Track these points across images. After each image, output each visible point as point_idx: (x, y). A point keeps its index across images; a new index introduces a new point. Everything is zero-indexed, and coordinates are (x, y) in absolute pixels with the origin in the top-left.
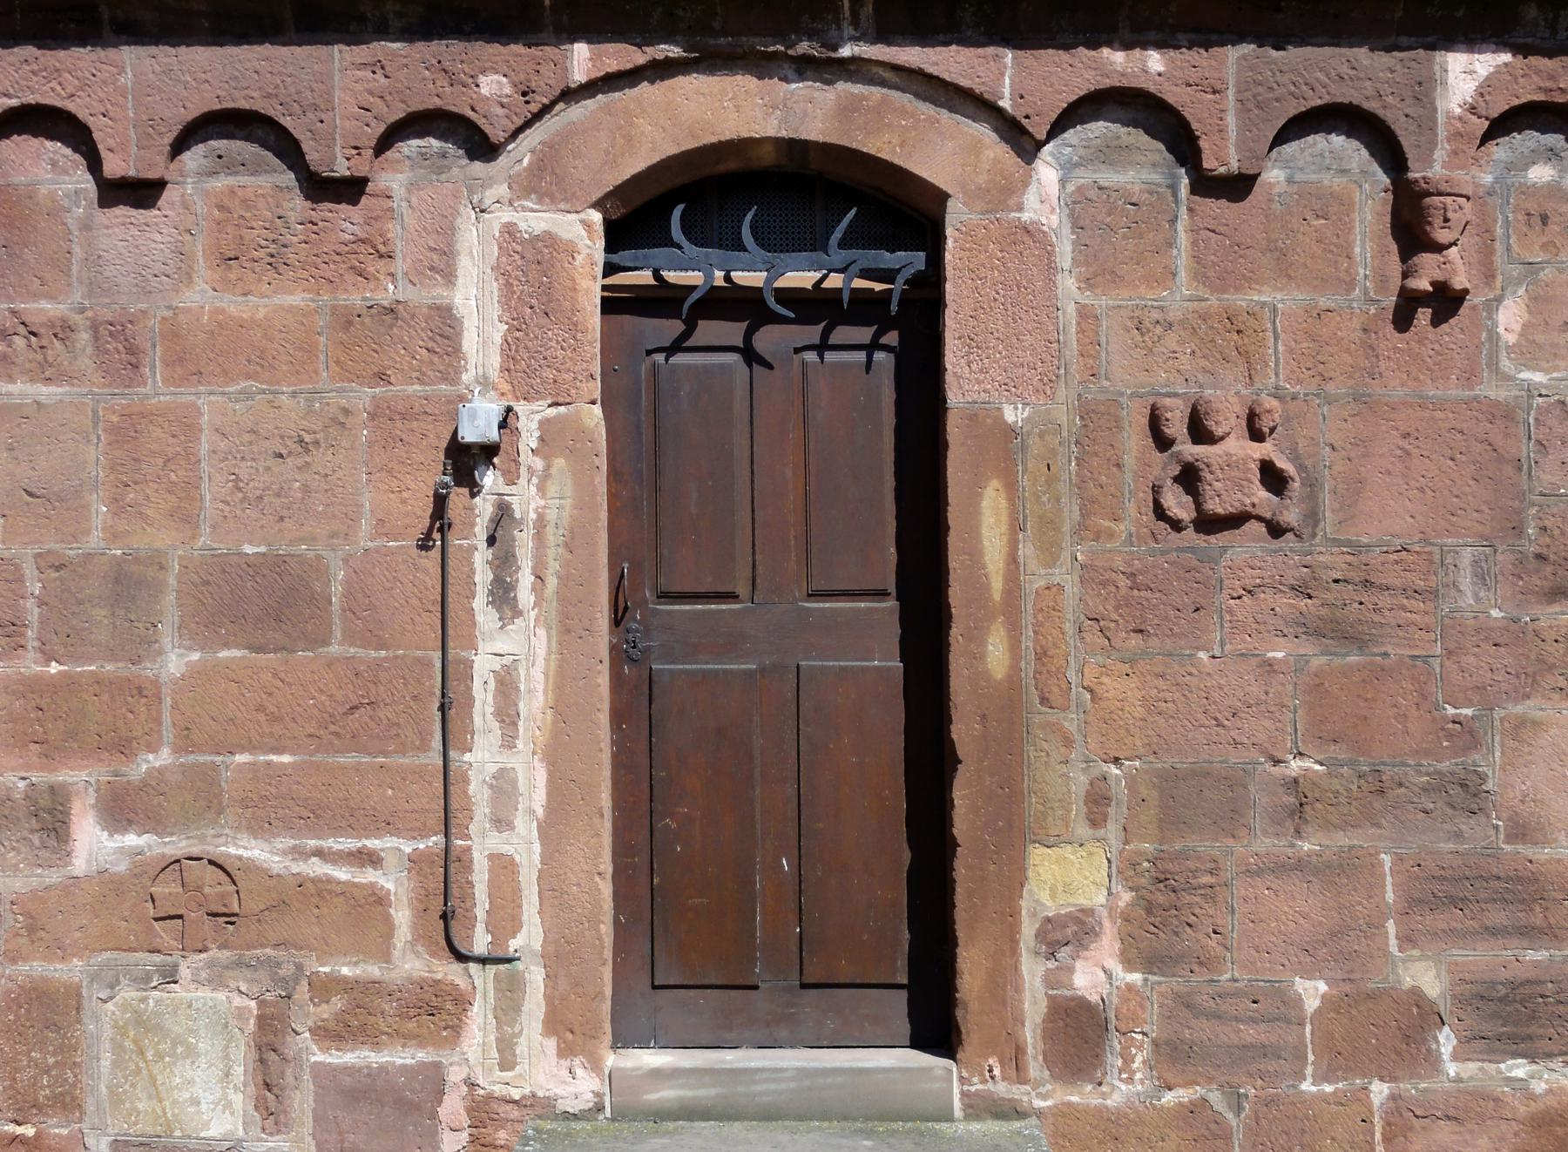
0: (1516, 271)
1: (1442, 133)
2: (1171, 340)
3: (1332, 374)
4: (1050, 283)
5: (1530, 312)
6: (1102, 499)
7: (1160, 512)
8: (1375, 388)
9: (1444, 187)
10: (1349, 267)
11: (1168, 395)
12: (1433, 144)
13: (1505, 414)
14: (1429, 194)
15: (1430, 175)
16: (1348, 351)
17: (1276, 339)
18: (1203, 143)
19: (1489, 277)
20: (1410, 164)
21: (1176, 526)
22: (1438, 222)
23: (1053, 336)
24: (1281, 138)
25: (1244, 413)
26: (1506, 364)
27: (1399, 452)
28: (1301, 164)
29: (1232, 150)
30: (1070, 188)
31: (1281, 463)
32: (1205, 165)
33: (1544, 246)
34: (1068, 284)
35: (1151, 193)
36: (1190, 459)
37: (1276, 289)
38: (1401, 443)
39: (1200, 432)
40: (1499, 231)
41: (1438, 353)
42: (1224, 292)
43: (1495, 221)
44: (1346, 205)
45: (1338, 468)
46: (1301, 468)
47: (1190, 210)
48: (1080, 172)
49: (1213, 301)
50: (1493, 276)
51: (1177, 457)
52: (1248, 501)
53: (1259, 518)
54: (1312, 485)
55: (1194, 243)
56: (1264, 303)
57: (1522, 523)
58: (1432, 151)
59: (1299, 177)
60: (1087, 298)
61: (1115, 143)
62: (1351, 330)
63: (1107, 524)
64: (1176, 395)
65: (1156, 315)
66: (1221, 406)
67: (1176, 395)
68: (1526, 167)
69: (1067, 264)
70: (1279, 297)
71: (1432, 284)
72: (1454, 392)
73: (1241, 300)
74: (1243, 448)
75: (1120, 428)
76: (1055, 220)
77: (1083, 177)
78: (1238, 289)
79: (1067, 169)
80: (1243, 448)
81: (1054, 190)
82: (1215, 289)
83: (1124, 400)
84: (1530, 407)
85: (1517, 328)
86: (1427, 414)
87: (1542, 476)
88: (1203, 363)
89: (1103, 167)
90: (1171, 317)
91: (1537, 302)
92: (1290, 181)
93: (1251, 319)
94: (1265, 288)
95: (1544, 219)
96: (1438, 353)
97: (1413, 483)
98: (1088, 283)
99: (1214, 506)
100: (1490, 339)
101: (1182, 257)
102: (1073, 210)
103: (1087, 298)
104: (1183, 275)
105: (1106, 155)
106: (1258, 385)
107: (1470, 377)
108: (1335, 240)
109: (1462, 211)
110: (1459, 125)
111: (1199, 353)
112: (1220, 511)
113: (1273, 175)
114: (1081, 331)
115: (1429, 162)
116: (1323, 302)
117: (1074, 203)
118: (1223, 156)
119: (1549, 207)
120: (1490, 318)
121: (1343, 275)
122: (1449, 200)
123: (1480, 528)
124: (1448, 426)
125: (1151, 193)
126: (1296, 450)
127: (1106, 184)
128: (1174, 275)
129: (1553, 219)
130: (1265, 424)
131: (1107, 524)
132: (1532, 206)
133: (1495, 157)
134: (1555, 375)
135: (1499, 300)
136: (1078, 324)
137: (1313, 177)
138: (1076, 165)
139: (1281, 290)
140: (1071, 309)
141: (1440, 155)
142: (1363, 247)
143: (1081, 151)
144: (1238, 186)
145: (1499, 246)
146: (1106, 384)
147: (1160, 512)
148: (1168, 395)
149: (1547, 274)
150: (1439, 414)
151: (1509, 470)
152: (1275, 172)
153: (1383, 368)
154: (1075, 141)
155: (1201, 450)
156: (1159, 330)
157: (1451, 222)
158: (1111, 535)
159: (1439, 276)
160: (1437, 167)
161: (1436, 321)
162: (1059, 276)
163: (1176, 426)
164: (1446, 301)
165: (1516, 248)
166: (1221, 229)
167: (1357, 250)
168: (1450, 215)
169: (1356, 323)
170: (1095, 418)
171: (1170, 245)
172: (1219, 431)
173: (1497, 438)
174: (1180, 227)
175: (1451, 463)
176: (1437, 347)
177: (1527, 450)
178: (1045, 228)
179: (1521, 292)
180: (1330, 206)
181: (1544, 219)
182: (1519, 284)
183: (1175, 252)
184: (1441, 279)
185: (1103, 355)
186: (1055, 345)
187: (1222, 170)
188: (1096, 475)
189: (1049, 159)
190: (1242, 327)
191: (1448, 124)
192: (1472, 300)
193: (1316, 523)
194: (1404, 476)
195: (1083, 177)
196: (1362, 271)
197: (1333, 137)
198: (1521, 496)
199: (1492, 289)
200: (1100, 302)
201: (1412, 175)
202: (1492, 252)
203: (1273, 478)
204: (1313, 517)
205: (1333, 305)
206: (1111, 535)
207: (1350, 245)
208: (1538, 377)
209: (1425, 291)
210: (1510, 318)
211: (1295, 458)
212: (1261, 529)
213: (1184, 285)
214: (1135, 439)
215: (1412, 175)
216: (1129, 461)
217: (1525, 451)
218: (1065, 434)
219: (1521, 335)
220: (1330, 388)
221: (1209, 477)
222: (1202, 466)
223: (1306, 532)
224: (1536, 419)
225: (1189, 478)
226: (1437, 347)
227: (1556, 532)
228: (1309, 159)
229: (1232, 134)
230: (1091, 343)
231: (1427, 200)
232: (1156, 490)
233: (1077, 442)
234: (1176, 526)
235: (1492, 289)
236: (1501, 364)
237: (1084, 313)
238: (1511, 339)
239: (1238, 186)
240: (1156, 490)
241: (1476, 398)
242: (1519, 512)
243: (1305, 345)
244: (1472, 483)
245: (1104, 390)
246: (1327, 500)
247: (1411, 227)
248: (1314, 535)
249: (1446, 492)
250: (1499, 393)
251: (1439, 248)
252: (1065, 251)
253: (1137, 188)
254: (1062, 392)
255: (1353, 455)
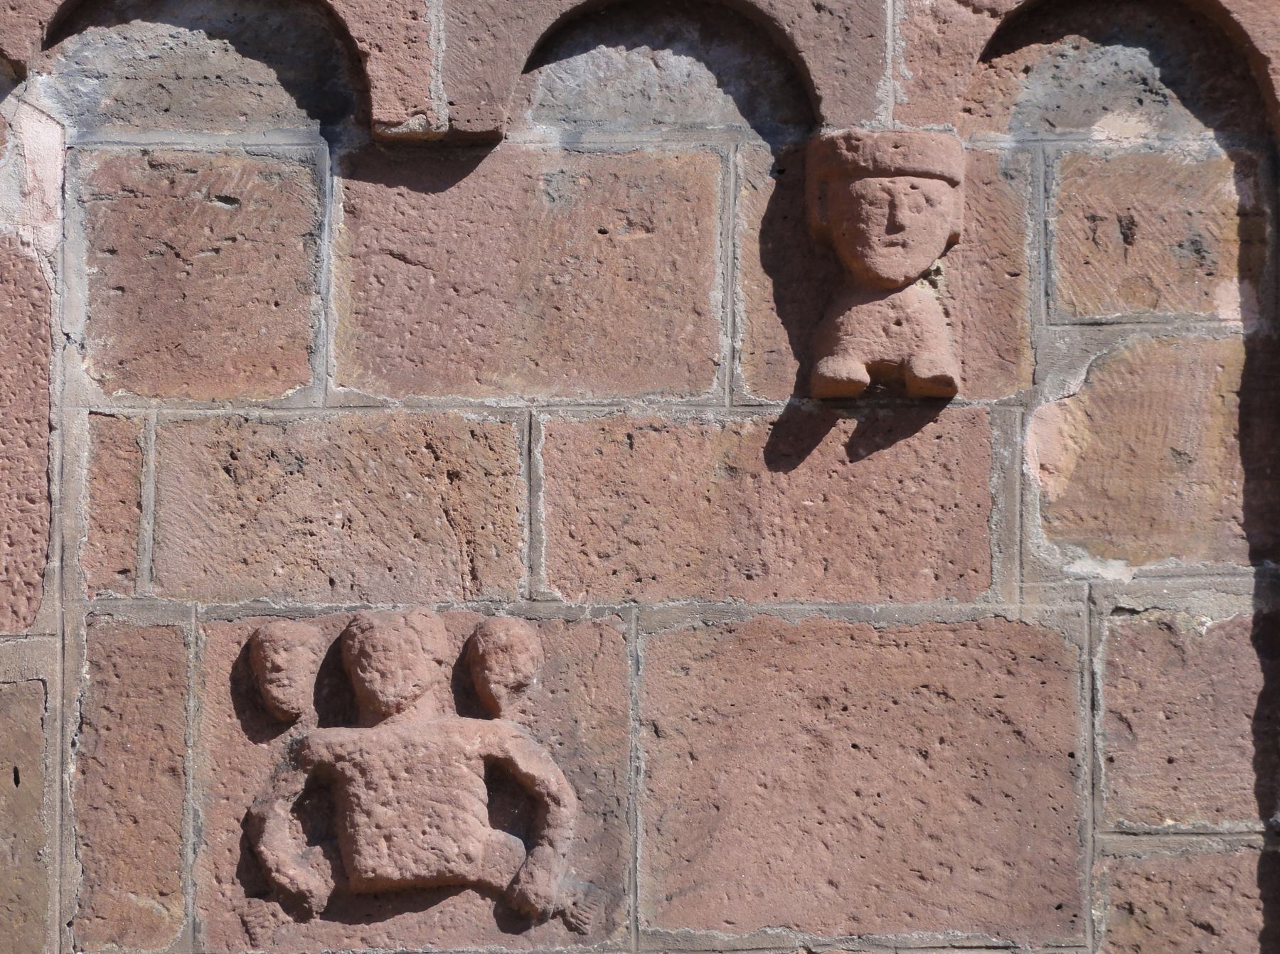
0: (1064, 339)
1: (894, 42)
2: (301, 496)
3: (656, 567)
4: (36, 371)
5: (1095, 430)
6: (133, 846)
7: (256, 877)
8: (755, 602)
9: (889, 157)
10: (698, 331)
11: (290, 615)
12: (874, 67)
13: (1039, 654)
14: (864, 173)
15: (858, 131)
16: (693, 516)
17: (533, 489)
18: (374, 68)
19: (1007, 354)
20: (825, 109)
21: (297, 905)
22: (876, 232)
23: (37, 487)
24: (549, 49)
25: (450, 652)
26: (1039, 540)
27: (804, 739)
28: (596, 111)
29: (437, 83)
30: (89, 165)
31: (536, 763)
32: (378, 114)
33: (1127, 288)
34: (76, 375)
35: (267, 175)
36: (327, 756)
37: (533, 379)
38: (807, 716)
39: (346, 691)
40: (1030, 255)
41: (893, 520)
42: (422, 388)
43: (1020, 233)
44: (693, 199)
45: (664, 778)
46: (581, 775)
47: (351, 211)
48: (114, 132)
49: (397, 407)
50: (1017, 351)
51: (298, 755)
52: (452, 849)
53: (483, 888)
54: (607, 815)
55: (359, 283)
56: (509, 412)
57: (1077, 896)
58: (871, 82)
59: (591, 138)
60: (120, 403)
61: (192, 70)
62: (699, 467)
63: (145, 902)
64: (308, 615)
65: (269, 439)
66: (393, 638)
67: (308, 615)
68: (1089, 117)
69: (77, 331)
70: (542, 398)
71: (873, 368)
72: (929, 605)
73: (463, 407)
74: (445, 730)
75: (181, 689)
76: (50, 234)
77: (120, 141)
78: (452, 382)
79: (87, 120)
80: (445, 730)
81: (52, 170)
82: (398, 384)
83: (190, 626)
84: (1095, 636)
85: (1067, 462)
86: (866, 654)
87: (1123, 789)
88: (367, 541)
89: (161, 118)
90: (302, 442)
91: (1104, 407)
92: (572, 148)
93: (479, 448)
94: (512, 380)
95: (1128, 231)
96: (893, 520)
97: (832, 807)
98: (121, 371)
99: (378, 860)
100: (1007, 486)
101: (331, 312)
102: (92, 213)
103: (120, 403)
104: (330, 351)
105: (163, 96)
106: (490, 591)
107: (960, 573)
108: (668, 275)
109: (933, 213)
110: (933, 27)
111: (360, 523)
112: (392, 872)
113: (533, 137)
114: (101, 474)
115: (868, 108)
116: (638, 411)
117: (97, 196)
118: (412, 90)
119: (1137, 201)
120: (1008, 442)
121: (682, 350)
122: (902, 184)
123: (984, 907)
124: (914, 680)
125: (267, 175)
126: (572, 735)
127: (168, 157)
128: (311, 351)
129: (1144, 227)
130: (498, 678)
131: (145, 902)
132: (1103, 203)
133: (1021, 96)
134: (1150, 567)
135: (1027, 404)
136: (96, 458)
137: (623, 140)
138: (108, 116)
139: (548, 383)
140: (79, 427)
141: (891, 88)
142: (728, 287)
143: (119, 87)
144: (445, 157)
145: (1029, 288)
146: (151, 589)
147: (256, 877)
148: (290, 615)
149: (1134, 344)
150: (894, 655)
151: (1048, 777)
152: (541, 129)
153: (769, 555)
154: (103, 63)
155: (344, 737)
156: (274, 472)
157: (921, 227)
158: (152, 929)
159: (886, 350)
160: (885, 116)
161: (855, 450)
162: (56, 358)
163: (296, 686)
164: (901, 403)
165: (1064, 289)
166: (420, 252)
167: (716, 295)
168: (904, 216)
169: (712, 457)
170: (130, 670)
171: (306, 288)
172: (388, 692)
173: (1024, 707)
174: (327, 247)
175: (919, 761)
176: (890, 505)
177: (1087, 732)
178: (30, 252)
179: (1075, 385)
180: (649, 206)
181: (1128, 231)
182: (1072, 367)
183: (315, 301)
184: (892, 356)
185: (147, 526)
186: (42, 506)
187: (415, 124)
188: (122, 793)
189: (48, 103)
190: (459, 464)
191: (908, 22)
192: (966, 401)
193: (616, 899)
194: (814, 791)
195: (120, 141)
196: (725, 342)
197: (667, 56)
198: (1075, 835)
199: (1012, 378)
200: (145, 411)
201: (828, 132)
202: (1013, 300)
203: (515, 800)
204: (608, 884)
205: (661, 416)
206: (152, 929)
207: (700, 285)
208: (1115, 572)
209: (859, 383)
210: (1048, 440)
211: (569, 752)
212: (483, 908)
213: (333, 374)
214: (210, 714)
215: (828, 132)
216: (198, 764)
217: (1085, 734)
218: (55, 702)
219: (1075, 478)
220: (653, 597)
221: (365, 795)
222: (350, 771)
223: (592, 919)
224: (1110, 664)
225: (326, 805)
226: (890, 505)
227: (1155, 914)
228: (616, 101)
229: (438, 46)
230: (124, 500)
231: (858, 186)
232: (253, 827)
233: (83, 721)
234: (297, 905)
235: (1012, 378)
236: (1030, 545)
237: (113, 437)
238: (1055, 487)
239: (445, 157)
240: (253, 827)
241: (976, 621)
242: (1071, 870)
243: (596, 503)
244: (965, 805)
245: (146, 605)
246: (642, 849)
247: (818, 248)
248: (609, 927)
249: (908, 827)
250: (1013, 602)
251: (886, 288)
252: (72, 301)
253: (236, 166)
254: (52, 605)
255: (699, 747)
